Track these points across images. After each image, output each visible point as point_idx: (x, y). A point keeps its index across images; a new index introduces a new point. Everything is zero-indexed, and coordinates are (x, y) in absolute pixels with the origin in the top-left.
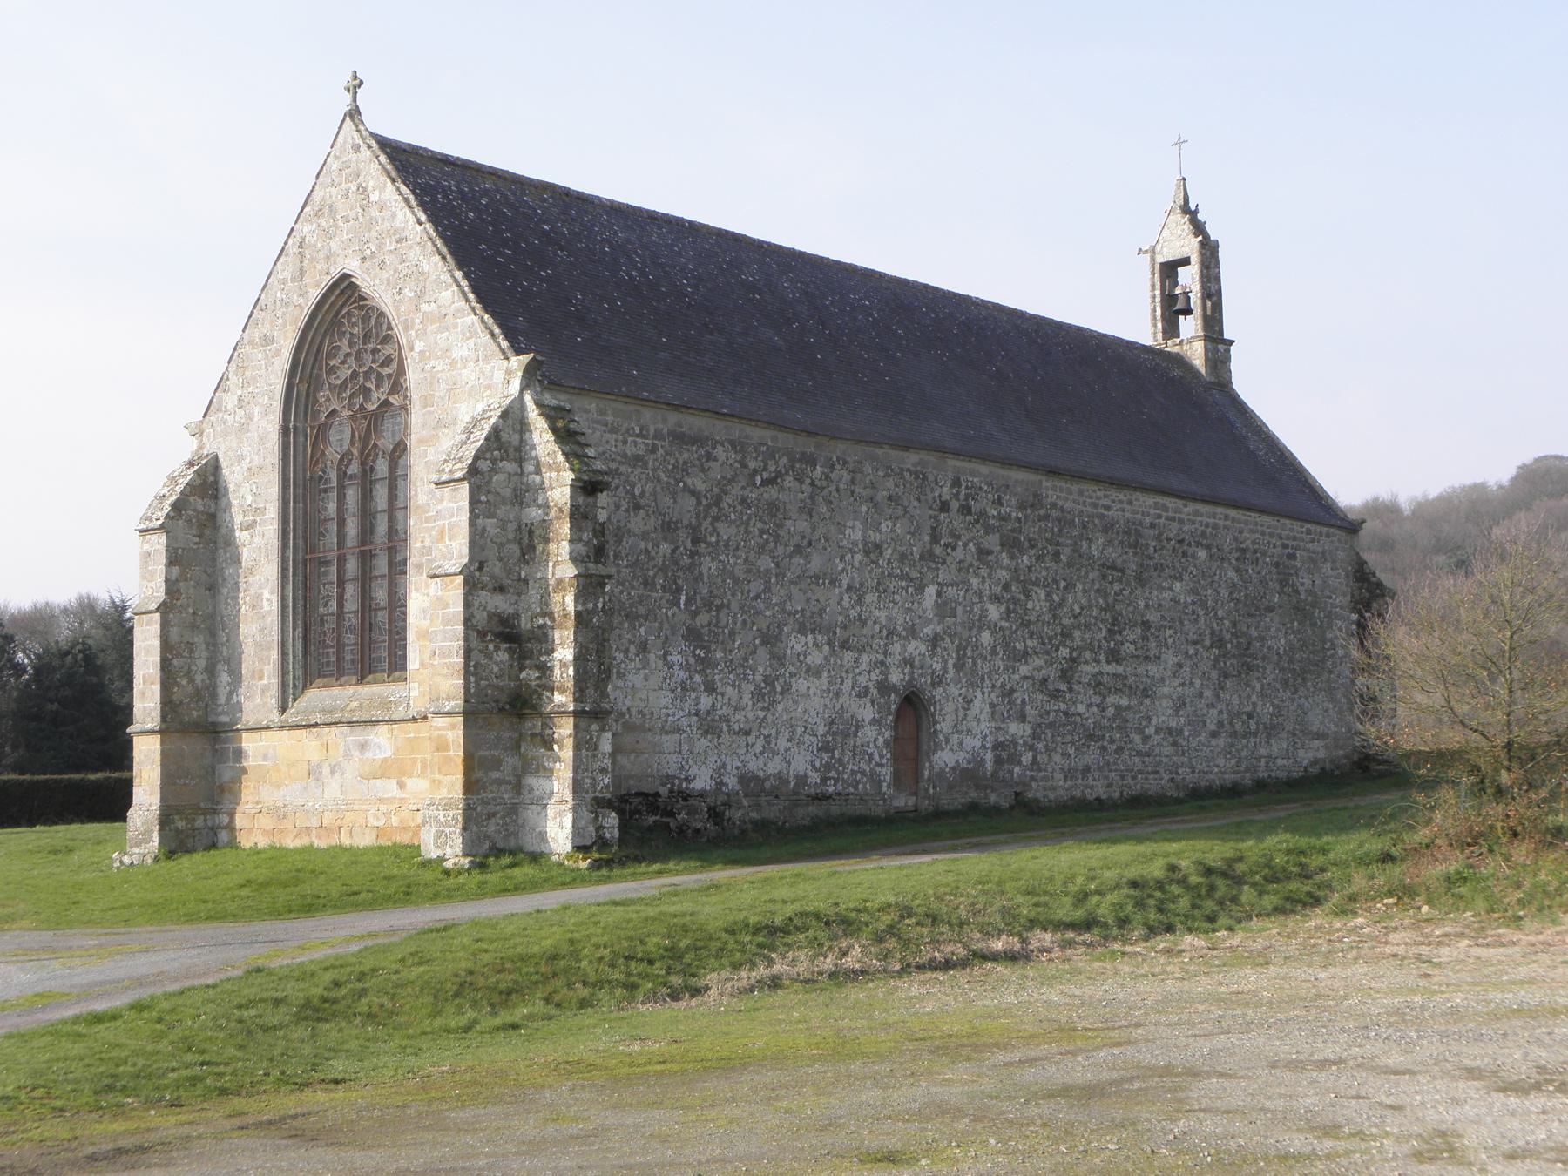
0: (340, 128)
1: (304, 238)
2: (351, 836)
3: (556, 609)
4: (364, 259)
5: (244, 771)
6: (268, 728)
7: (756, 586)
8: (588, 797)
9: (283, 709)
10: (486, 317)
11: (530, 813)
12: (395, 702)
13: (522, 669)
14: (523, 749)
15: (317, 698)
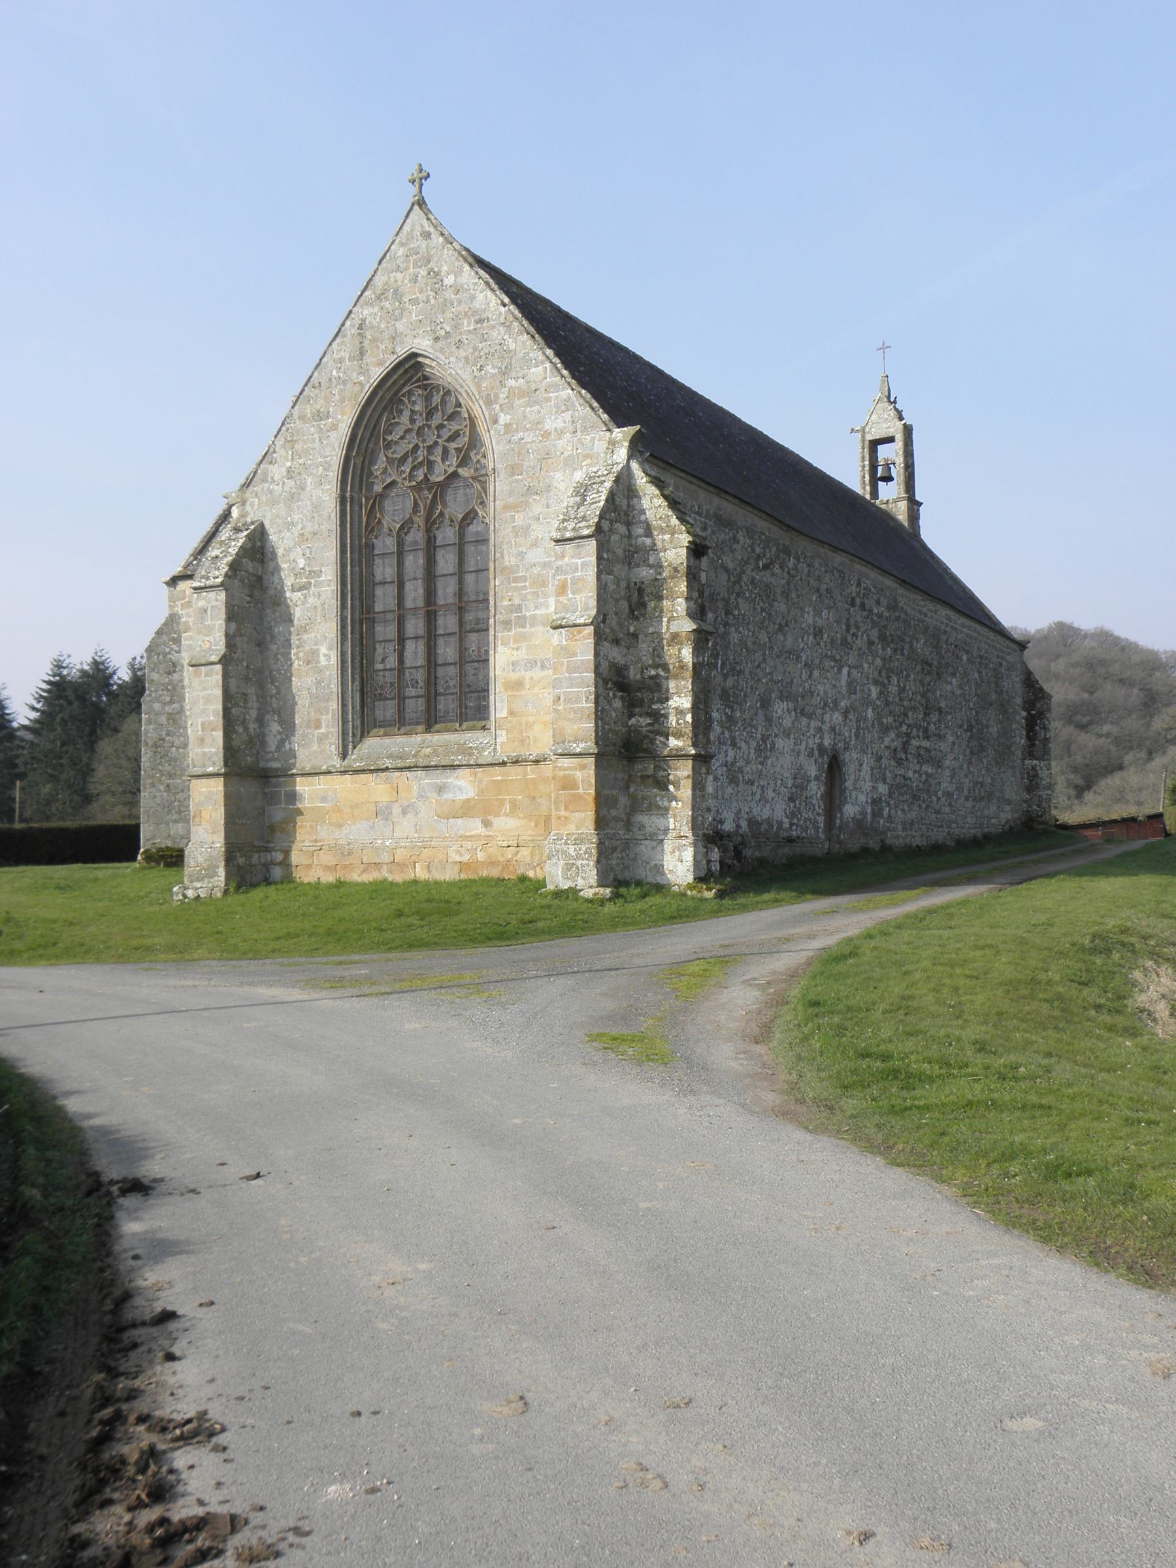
0: (407, 216)
1: (364, 320)
2: (429, 871)
3: (671, 662)
4: (437, 339)
5: (299, 812)
6: (329, 773)
7: (758, 657)
8: (700, 833)
9: (344, 756)
10: (583, 391)
11: (644, 848)
12: (476, 748)
13: (631, 715)
14: (632, 790)
15: (374, 745)
